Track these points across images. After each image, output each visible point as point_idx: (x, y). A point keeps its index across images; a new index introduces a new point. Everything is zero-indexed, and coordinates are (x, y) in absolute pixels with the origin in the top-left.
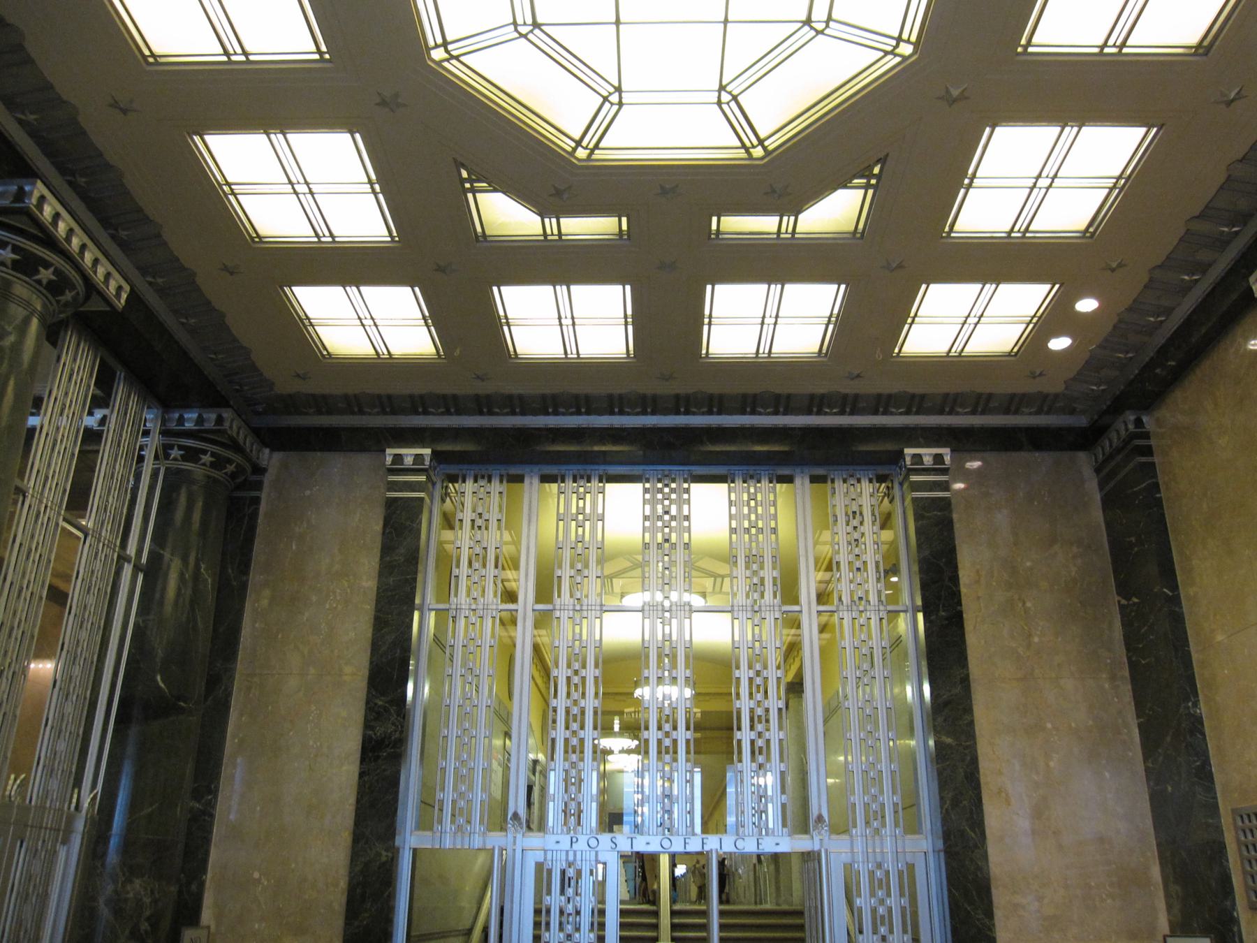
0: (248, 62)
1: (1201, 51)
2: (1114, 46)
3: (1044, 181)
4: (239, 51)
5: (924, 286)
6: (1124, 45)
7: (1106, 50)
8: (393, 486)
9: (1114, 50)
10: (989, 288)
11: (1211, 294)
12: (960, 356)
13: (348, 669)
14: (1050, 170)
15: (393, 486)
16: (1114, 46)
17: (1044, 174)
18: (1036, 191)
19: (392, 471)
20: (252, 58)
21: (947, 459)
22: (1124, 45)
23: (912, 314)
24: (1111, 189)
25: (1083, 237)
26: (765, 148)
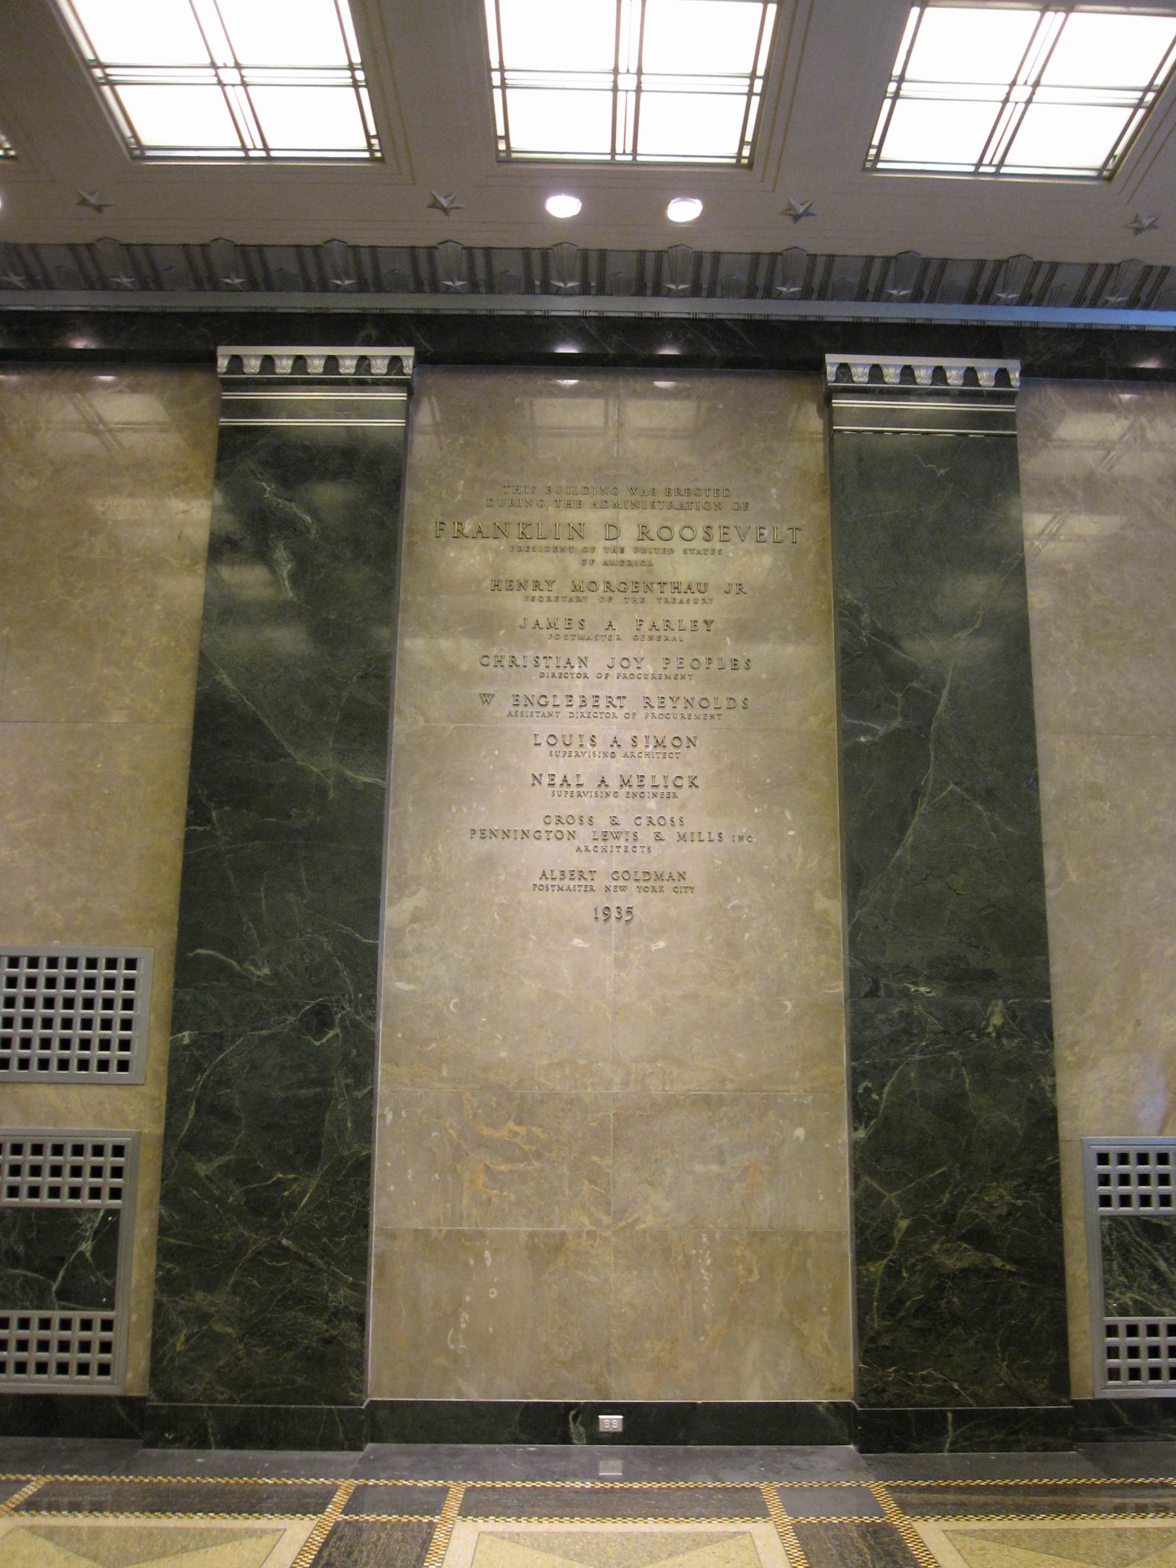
0: (269, 158)
1: (1105, 173)
2: (990, 164)
3: (1022, 93)
4: (259, 145)
5: (915, 11)
6: (1001, 163)
7: (982, 169)
8: (230, 408)
9: (992, 170)
10: (1054, 19)
11: (97, 1507)
12: (997, 174)
13: (608, 983)
14: (1029, 73)
15: (230, 408)
16: (990, 164)
17: (1020, 81)
18: (1010, 106)
19: (229, 385)
20: (273, 154)
21: (1015, 376)
22: (1001, 163)
23: (875, 142)
24: (1136, 107)
25: (1099, 177)
26: (634, 158)
